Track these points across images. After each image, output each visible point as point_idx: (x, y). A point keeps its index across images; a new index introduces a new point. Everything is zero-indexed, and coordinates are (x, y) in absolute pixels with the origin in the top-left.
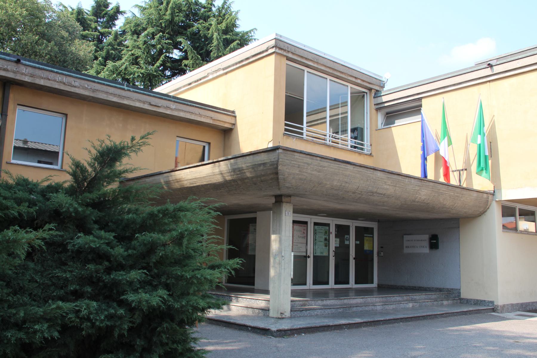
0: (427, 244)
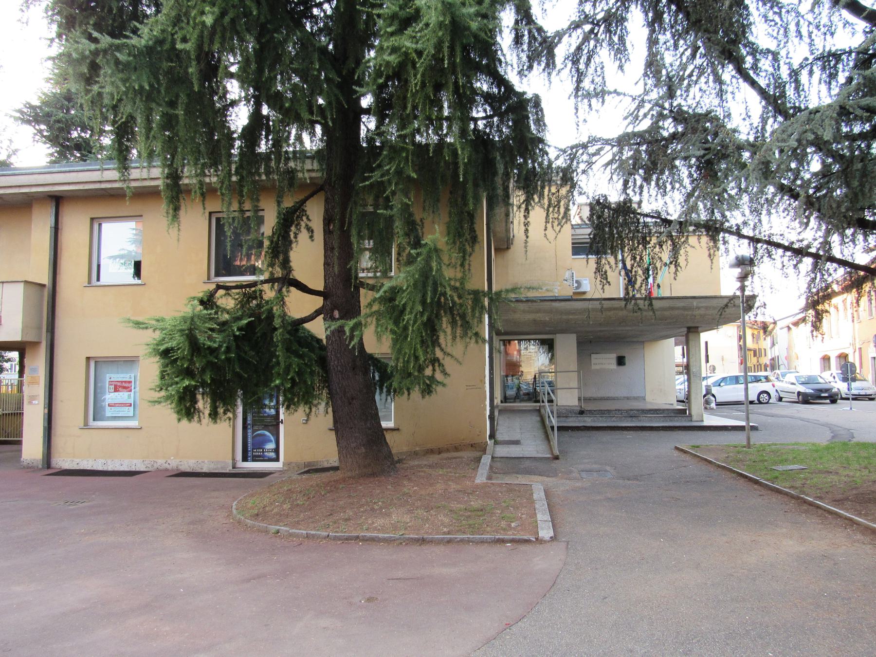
0: (614, 361)
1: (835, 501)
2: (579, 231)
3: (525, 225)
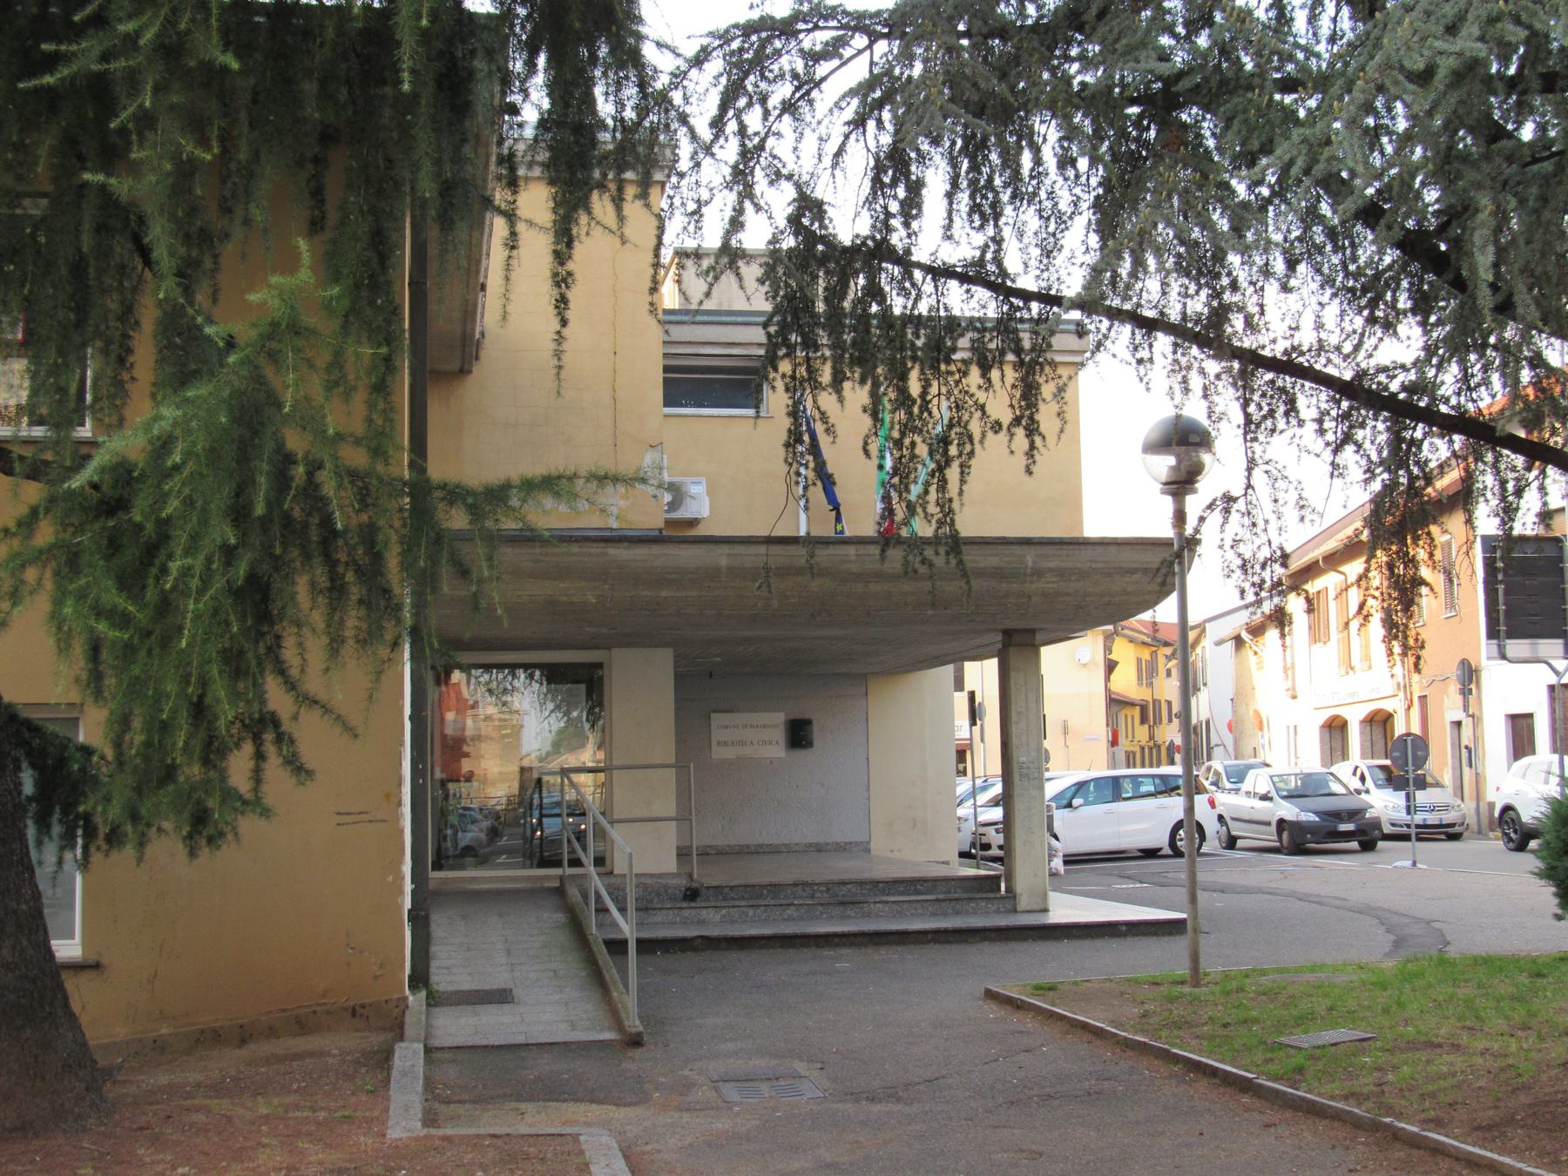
0: (779, 735)
1: (1479, 1128)
2: (678, 333)
3: (558, 285)
